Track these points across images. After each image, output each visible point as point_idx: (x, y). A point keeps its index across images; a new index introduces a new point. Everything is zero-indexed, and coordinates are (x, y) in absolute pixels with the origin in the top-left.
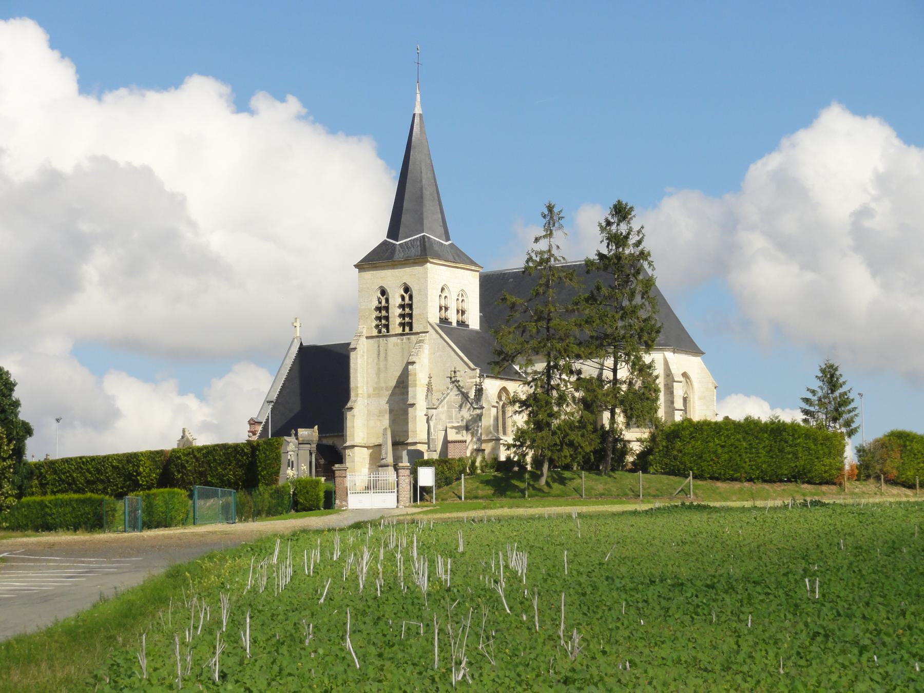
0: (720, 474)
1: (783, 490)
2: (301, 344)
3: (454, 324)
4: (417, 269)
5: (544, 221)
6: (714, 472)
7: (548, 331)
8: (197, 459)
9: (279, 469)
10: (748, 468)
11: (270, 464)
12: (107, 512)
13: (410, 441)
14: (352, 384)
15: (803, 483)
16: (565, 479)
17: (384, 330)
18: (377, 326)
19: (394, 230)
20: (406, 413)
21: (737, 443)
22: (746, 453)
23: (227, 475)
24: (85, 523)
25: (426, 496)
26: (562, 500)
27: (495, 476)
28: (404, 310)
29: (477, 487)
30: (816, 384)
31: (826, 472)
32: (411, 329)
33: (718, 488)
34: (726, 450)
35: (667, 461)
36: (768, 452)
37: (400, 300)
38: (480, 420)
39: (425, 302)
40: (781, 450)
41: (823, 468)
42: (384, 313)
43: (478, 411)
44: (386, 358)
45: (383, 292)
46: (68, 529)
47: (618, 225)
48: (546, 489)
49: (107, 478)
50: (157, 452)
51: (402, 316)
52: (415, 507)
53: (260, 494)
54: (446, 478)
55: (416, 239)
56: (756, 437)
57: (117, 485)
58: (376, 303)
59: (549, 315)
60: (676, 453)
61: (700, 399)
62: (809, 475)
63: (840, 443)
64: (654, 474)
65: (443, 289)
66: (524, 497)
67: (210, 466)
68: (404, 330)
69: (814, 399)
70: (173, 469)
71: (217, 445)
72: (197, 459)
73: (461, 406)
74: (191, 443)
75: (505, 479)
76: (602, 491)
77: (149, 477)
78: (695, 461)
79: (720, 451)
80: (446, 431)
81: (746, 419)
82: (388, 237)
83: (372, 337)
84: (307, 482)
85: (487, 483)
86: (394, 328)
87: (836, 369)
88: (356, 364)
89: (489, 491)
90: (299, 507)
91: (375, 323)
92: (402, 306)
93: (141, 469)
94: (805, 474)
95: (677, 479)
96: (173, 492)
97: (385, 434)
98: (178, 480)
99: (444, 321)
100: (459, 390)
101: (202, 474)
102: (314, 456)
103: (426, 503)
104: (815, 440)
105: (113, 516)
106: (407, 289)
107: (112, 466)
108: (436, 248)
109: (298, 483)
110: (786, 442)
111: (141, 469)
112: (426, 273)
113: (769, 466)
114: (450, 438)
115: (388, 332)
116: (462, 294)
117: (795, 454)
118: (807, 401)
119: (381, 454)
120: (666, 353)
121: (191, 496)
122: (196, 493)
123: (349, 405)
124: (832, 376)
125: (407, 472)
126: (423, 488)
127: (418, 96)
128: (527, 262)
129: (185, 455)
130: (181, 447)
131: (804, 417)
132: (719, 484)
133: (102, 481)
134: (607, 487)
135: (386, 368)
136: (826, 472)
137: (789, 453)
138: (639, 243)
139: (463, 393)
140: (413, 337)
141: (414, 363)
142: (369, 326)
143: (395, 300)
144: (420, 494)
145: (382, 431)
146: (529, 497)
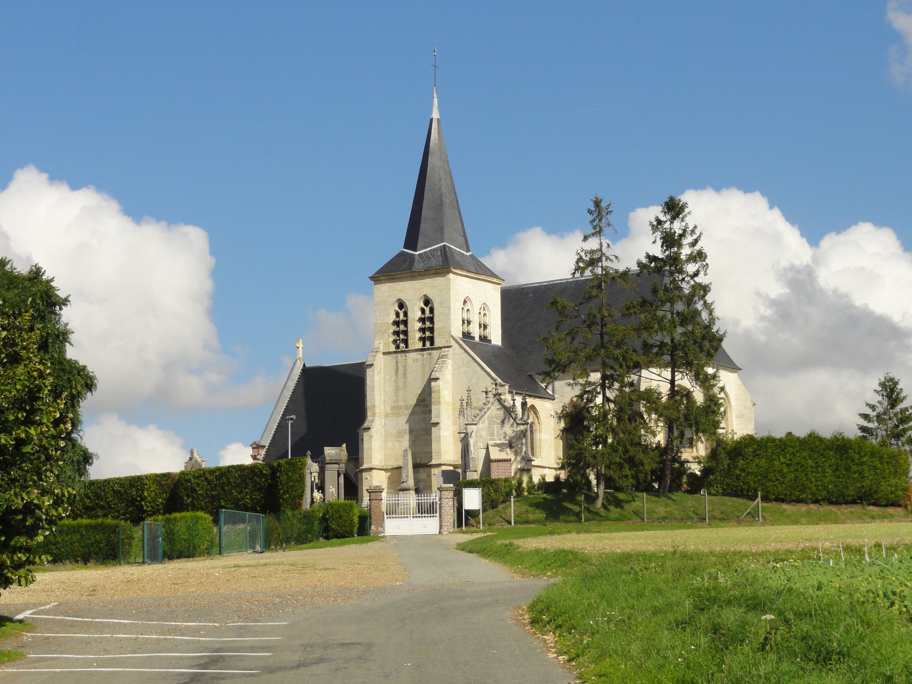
0: (786, 495)
2: (304, 365)
3: (477, 339)
4: (438, 281)
5: (591, 218)
6: (780, 493)
7: (602, 337)
8: (209, 482)
10: (814, 488)
11: (293, 486)
12: (123, 540)
13: (434, 462)
14: (369, 404)
15: (869, 505)
17: (402, 345)
18: (395, 341)
19: (412, 241)
20: (429, 433)
21: (803, 462)
23: (243, 498)
24: (97, 554)
25: (472, 521)
26: (622, 524)
27: (544, 498)
28: (424, 323)
29: (527, 511)
30: (875, 399)
31: (892, 493)
32: (432, 344)
33: (785, 510)
35: (728, 480)
36: (834, 471)
39: (448, 315)
40: (848, 469)
41: (889, 489)
42: (402, 327)
43: (522, 428)
45: (401, 305)
46: (77, 562)
47: (672, 223)
48: (603, 512)
49: (108, 503)
50: (164, 475)
51: (422, 330)
52: (459, 532)
54: (492, 501)
56: (822, 455)
57: (118, 511)
58: (393, 317)
59: (602, 320)
60: (738, 472)
61: (738, 417)
62: (875, 497)
63: (906, 462)
65: (465, 302)
68: (424, 345)
69: (873, 414)
70: (183, 493)
71: (232, 467)
72: (209, 482)
73: (503, 422)
74: (200, 465)
75: (559, 502)
77: (154, 502)
78: (759, 481)
79: (785, 470)
80: (487, 449)
81: (810, 435)
82: (405, 247)
83: (390, 353)
84: (340, 506)
85: (537, 505)
86: (414, 344)
87: (896, 383)
88: (373, 381)
89: (540, 515)
90: (331, 534)
91: (392, 338)
92: (422, 320)
93: (146, 494)
94: (871, 495)
95: (740, 501)
96: (197, 517)
99: (467, 336)
100: (501, 403)
102: (342, 477)
104: (881, 458)
105: (130, 545)
106: (427, 302)
107: (114, 491)
108: (458, 258)
111: (146, 494)
112: (448, 284)
113: (836, 486)
114: (493, 457)
115: (407, 347)
116: (485, 307)
117: (861, 473)
118: (866, 417)
119: (400, 477)
121: (216, 521)
122: (222, 516)
123: (365, 425)
124: (892, 390)
125: (451, 494)
126: (468, 512)
127: (436, 100)
128: (577, 263)
129: (195, 478)
130: (189, 469)
132: (785, 506)
133: (102, 507)
134: (669, 509)
135: (405, 386)
136: (892, 493)
137: (855, 473)
139: (505, 407)
141: (437, 379)
142: (385, 341)
143: (415, 314)
144: (464, 518)
146: (586, 521)
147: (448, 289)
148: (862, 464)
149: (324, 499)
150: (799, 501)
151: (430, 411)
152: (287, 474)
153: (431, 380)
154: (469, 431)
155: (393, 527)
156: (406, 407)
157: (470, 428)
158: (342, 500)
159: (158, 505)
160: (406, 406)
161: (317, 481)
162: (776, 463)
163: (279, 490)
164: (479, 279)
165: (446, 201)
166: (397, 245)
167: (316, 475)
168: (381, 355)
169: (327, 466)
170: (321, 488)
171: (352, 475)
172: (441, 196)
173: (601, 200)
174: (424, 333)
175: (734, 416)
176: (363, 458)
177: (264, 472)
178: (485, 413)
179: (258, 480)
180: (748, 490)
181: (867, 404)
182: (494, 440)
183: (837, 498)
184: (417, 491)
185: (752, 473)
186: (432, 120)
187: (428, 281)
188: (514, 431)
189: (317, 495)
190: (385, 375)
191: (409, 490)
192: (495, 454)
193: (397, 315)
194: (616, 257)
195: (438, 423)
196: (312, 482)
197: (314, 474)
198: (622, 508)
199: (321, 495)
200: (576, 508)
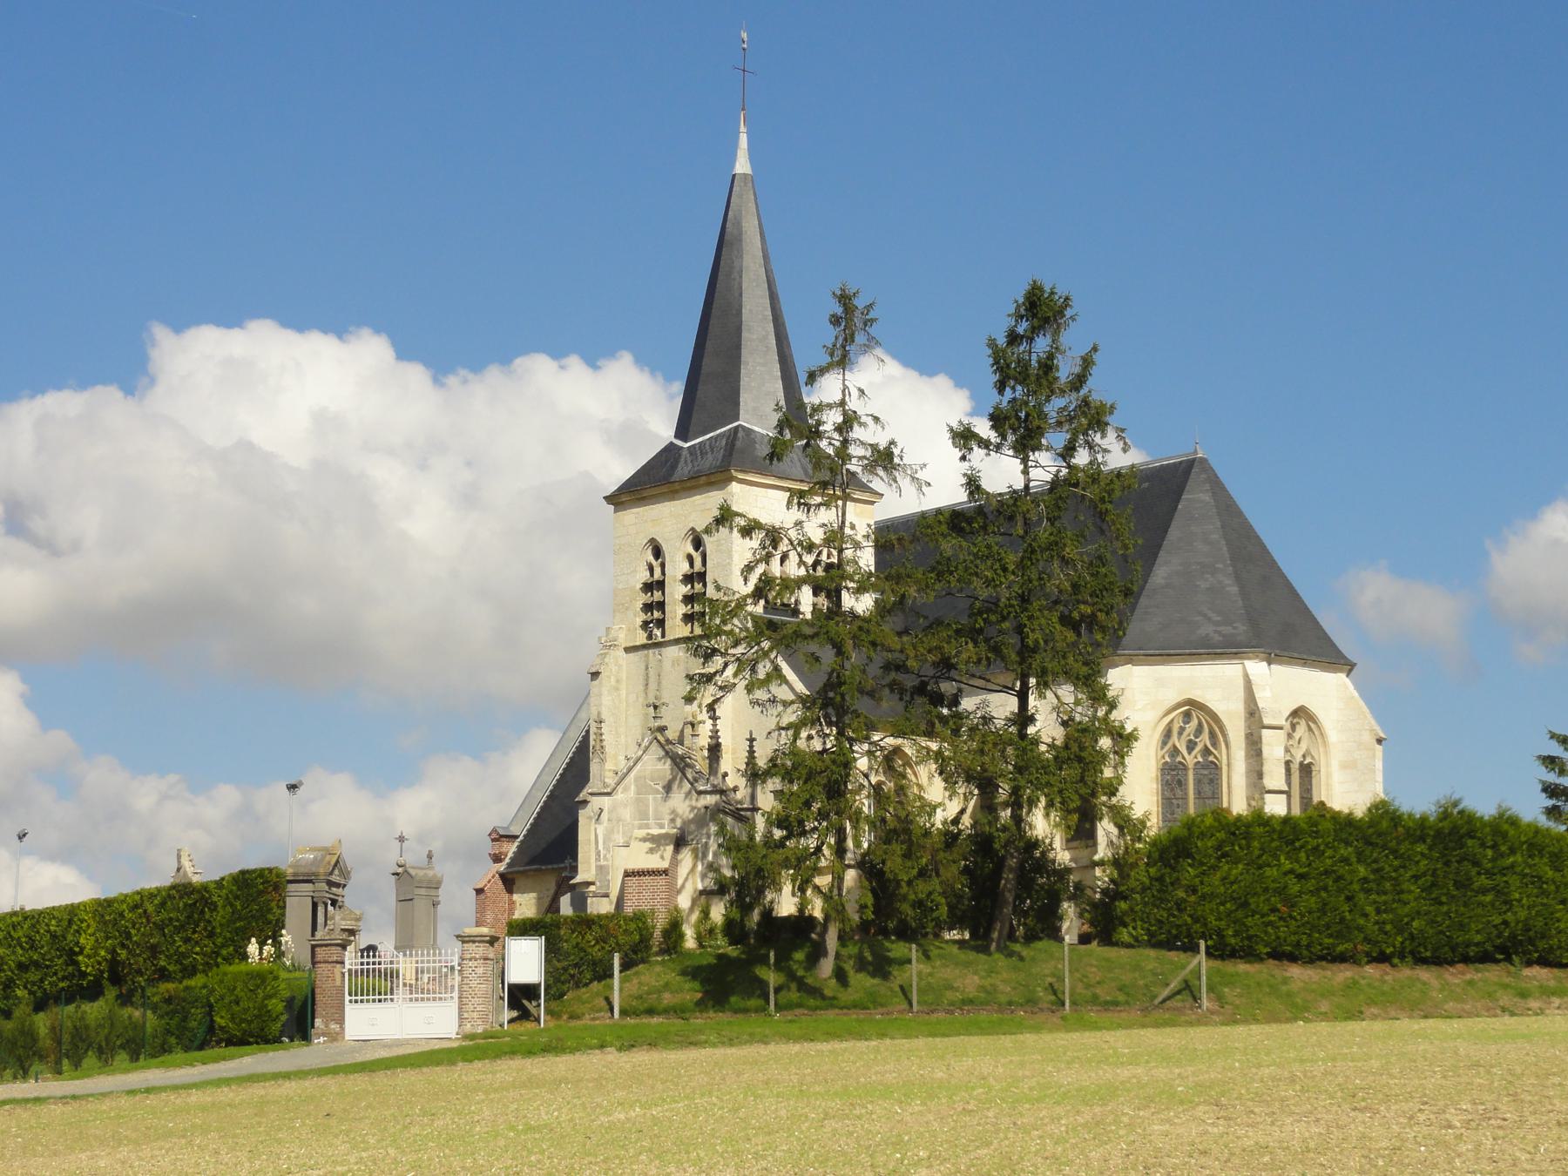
0: (1298, 944)
1: (1471, 983)
15: (1529, 964)
16: (890, 961)
18: (645, 625)
21: (1343, 870)
22: (1368, 891)
29: (667, 986)
33: (1285, 981)
34: (1311, 884)
36: (1426, 890)
37: (687, 565)
56: (1394, 852)
60: (1181, 894)
61: (1347, 766)
62: (1542, 945)
64: (1129, 946)
73: (668, 788)
76: (971, 992)
94: (1531, 941)
110: (1476, 863)
115: (663, 636)
118: (1550, 761)
120: (1246, 662)
127: (743, 140)
131: (1550, 803)
132: (1295, 971)
137: (1484, 891)
138: (1079, 381)
146: (778, 1008)
148: (1503, 871)
150: (1342, 959)
175: (1335, 764)
181: (1553, 736)
182: (647, 826)
183: (1435, 950)
185: (1213, 895)
188: (693, 808)
194: (876, 419)
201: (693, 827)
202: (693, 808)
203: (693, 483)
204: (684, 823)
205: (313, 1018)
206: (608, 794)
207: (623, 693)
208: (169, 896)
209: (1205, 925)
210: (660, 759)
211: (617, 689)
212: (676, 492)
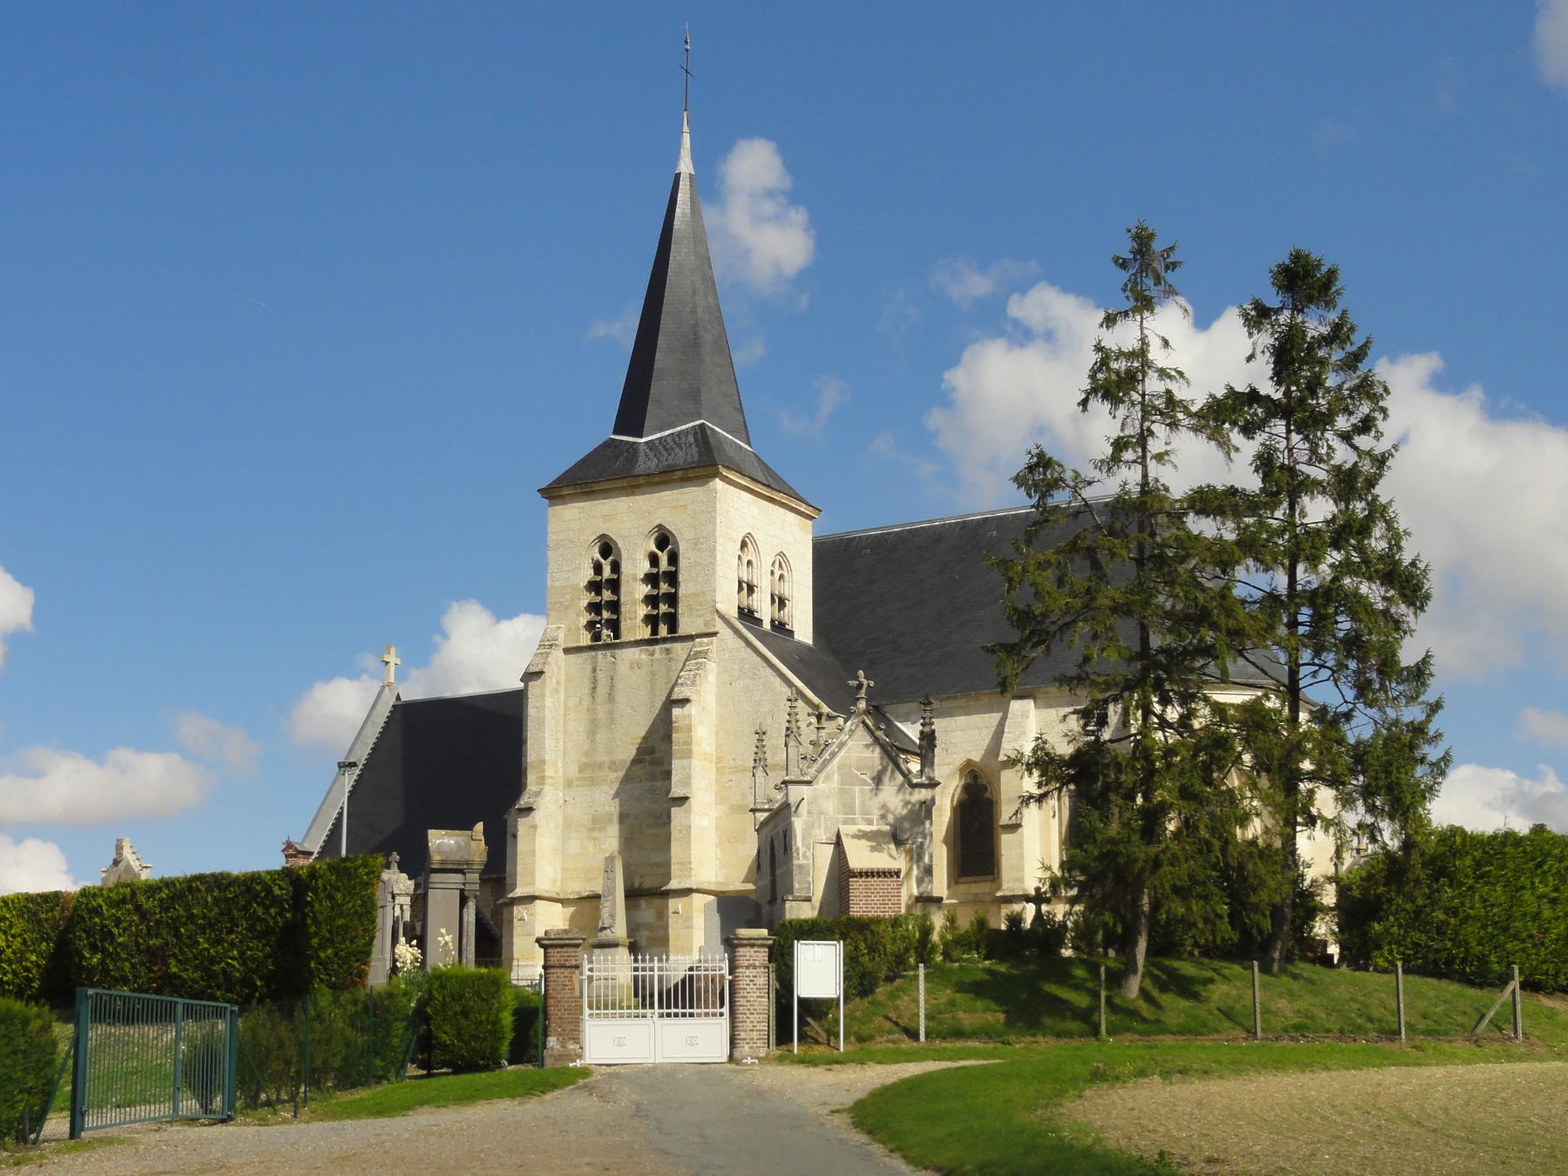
0: (1546, 973)
3: (767, 626)
4: (689, 495)
5: (1124, 276)
9: (370, 943)
11: (346, 928)
13: (674, 884)
14: (531, 755)
16: (1191, 980)
17: (606, 633)
18: (590, 625)
19: (631, 416)
28: (655, 585)
29: (952, 1003)
32: (673, 627)
35: (1415, 936)
38: (929, 815)
39: (709, 569)
43: (923, 794)
44: (611, 697)
45: (607, 548)
48: (1145, 1009)
51: (651, 600)
52: (781, 1060)
53: (319, 1017)
54: (863, 976)
55: (687, 432)
58: (588, 574)
60: (1440, 915)
65: (744, 545)
66: (1096, 1032)
67: (177, 935)
68: (655, 631)
70: (82, 943)
71: (200, 878)
72: (144, 916)
73: (878, 780)
77: (19, 961)
79: (1547, 913)
80: (838, 843)
83: (579, 650)
84: (466, 981)
85: (977, 989)
88: (542, 708)
90: (438, 1055)
91: (585, 618)
92: (652, 579)
97: (608, 871)
98: (91, 971)
99: (747, 615)
101: (155, 956)
102: (471, 905)
103: (818, 1050)
108: (731, 452)
109: (437, 985)
112: (713, 502)
115: (617, 636)
116: (782, 560)
123: (523, 802)
125: (762, 956)
127: (686, 139)
134: (1301, 1005)
135: (612, 720)
140: (677, 646)
141: (686, 701)
143: (636, 565)
144: (795, 1021)
145: (601, 864)
146: (1110, 1033)
147: (711, 512)
149: (423, 963)
151: (668, 775)
152: (330, 897)
153: (671, 703)
154: (793, 800)
155: (613, 1040)
156: (613, 766)
157: (795, 792)
158: (470, 966)
159: (27, 970)
160: (612, 763)
161: (407, 917)
162: (1527, 895)
163: (309, 937)
164: (772, 500)
165: (707, 338)
166: (602, 428)
167: (406, 901)
168: (561, 654)
169: (435, 877)
170: (417, 933)
171: (488, 915)
172: (695, 326)
173: (1152, 235)
174: (655, 606)
176: (514, 876)
177: (277, 891)
178: (833, 755)
179: (260, 911)
180: (1464, 960)
182: (853, 822)
184: (634, 948)
185: (1476, 918)
186: (678, 176)
187: (668, 496)
188: (907, 803)
189: (406, 952)
190: (567, 698)
191: (613, 945)
192: (860, 856)
193: (598, 568)
195: (686, 799)
196: (396, 922)
197: (399, 900)
198: (1195, 996)
199: (417, 951)
200: (1081, 1000)
201: (906, 825)
202: (907, 803)
203: (664, 477)
204: (896, 819)
205: (546, 1035)
206: (809, 783)
207: (562, 695)
208: (190, 889)
209: (1467, 950)
210: (867, 746)
211: (557, 691)
212: (638, 486)
